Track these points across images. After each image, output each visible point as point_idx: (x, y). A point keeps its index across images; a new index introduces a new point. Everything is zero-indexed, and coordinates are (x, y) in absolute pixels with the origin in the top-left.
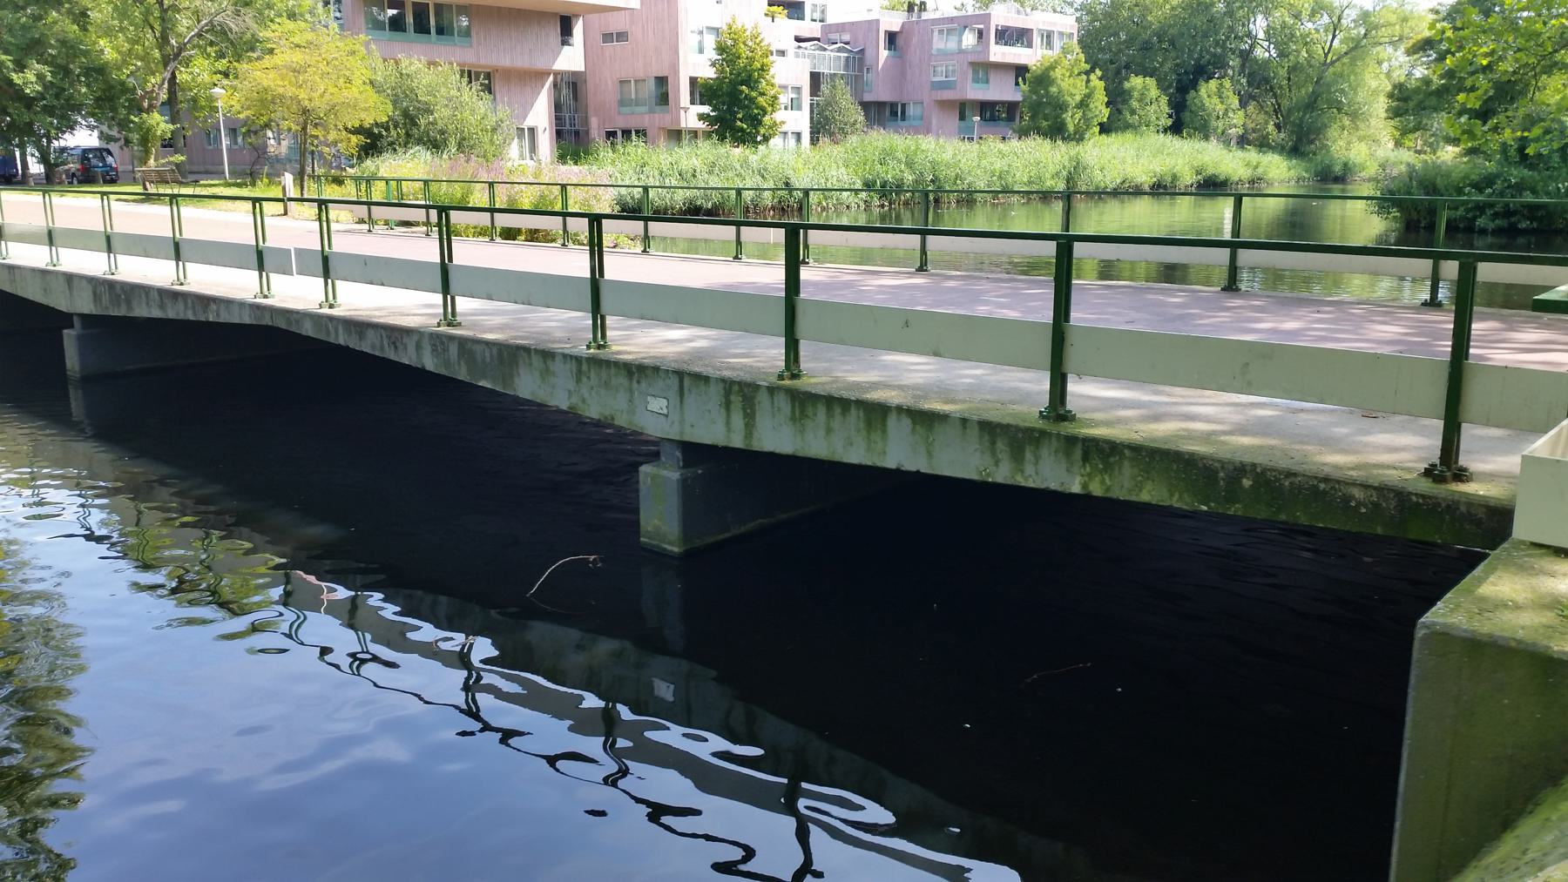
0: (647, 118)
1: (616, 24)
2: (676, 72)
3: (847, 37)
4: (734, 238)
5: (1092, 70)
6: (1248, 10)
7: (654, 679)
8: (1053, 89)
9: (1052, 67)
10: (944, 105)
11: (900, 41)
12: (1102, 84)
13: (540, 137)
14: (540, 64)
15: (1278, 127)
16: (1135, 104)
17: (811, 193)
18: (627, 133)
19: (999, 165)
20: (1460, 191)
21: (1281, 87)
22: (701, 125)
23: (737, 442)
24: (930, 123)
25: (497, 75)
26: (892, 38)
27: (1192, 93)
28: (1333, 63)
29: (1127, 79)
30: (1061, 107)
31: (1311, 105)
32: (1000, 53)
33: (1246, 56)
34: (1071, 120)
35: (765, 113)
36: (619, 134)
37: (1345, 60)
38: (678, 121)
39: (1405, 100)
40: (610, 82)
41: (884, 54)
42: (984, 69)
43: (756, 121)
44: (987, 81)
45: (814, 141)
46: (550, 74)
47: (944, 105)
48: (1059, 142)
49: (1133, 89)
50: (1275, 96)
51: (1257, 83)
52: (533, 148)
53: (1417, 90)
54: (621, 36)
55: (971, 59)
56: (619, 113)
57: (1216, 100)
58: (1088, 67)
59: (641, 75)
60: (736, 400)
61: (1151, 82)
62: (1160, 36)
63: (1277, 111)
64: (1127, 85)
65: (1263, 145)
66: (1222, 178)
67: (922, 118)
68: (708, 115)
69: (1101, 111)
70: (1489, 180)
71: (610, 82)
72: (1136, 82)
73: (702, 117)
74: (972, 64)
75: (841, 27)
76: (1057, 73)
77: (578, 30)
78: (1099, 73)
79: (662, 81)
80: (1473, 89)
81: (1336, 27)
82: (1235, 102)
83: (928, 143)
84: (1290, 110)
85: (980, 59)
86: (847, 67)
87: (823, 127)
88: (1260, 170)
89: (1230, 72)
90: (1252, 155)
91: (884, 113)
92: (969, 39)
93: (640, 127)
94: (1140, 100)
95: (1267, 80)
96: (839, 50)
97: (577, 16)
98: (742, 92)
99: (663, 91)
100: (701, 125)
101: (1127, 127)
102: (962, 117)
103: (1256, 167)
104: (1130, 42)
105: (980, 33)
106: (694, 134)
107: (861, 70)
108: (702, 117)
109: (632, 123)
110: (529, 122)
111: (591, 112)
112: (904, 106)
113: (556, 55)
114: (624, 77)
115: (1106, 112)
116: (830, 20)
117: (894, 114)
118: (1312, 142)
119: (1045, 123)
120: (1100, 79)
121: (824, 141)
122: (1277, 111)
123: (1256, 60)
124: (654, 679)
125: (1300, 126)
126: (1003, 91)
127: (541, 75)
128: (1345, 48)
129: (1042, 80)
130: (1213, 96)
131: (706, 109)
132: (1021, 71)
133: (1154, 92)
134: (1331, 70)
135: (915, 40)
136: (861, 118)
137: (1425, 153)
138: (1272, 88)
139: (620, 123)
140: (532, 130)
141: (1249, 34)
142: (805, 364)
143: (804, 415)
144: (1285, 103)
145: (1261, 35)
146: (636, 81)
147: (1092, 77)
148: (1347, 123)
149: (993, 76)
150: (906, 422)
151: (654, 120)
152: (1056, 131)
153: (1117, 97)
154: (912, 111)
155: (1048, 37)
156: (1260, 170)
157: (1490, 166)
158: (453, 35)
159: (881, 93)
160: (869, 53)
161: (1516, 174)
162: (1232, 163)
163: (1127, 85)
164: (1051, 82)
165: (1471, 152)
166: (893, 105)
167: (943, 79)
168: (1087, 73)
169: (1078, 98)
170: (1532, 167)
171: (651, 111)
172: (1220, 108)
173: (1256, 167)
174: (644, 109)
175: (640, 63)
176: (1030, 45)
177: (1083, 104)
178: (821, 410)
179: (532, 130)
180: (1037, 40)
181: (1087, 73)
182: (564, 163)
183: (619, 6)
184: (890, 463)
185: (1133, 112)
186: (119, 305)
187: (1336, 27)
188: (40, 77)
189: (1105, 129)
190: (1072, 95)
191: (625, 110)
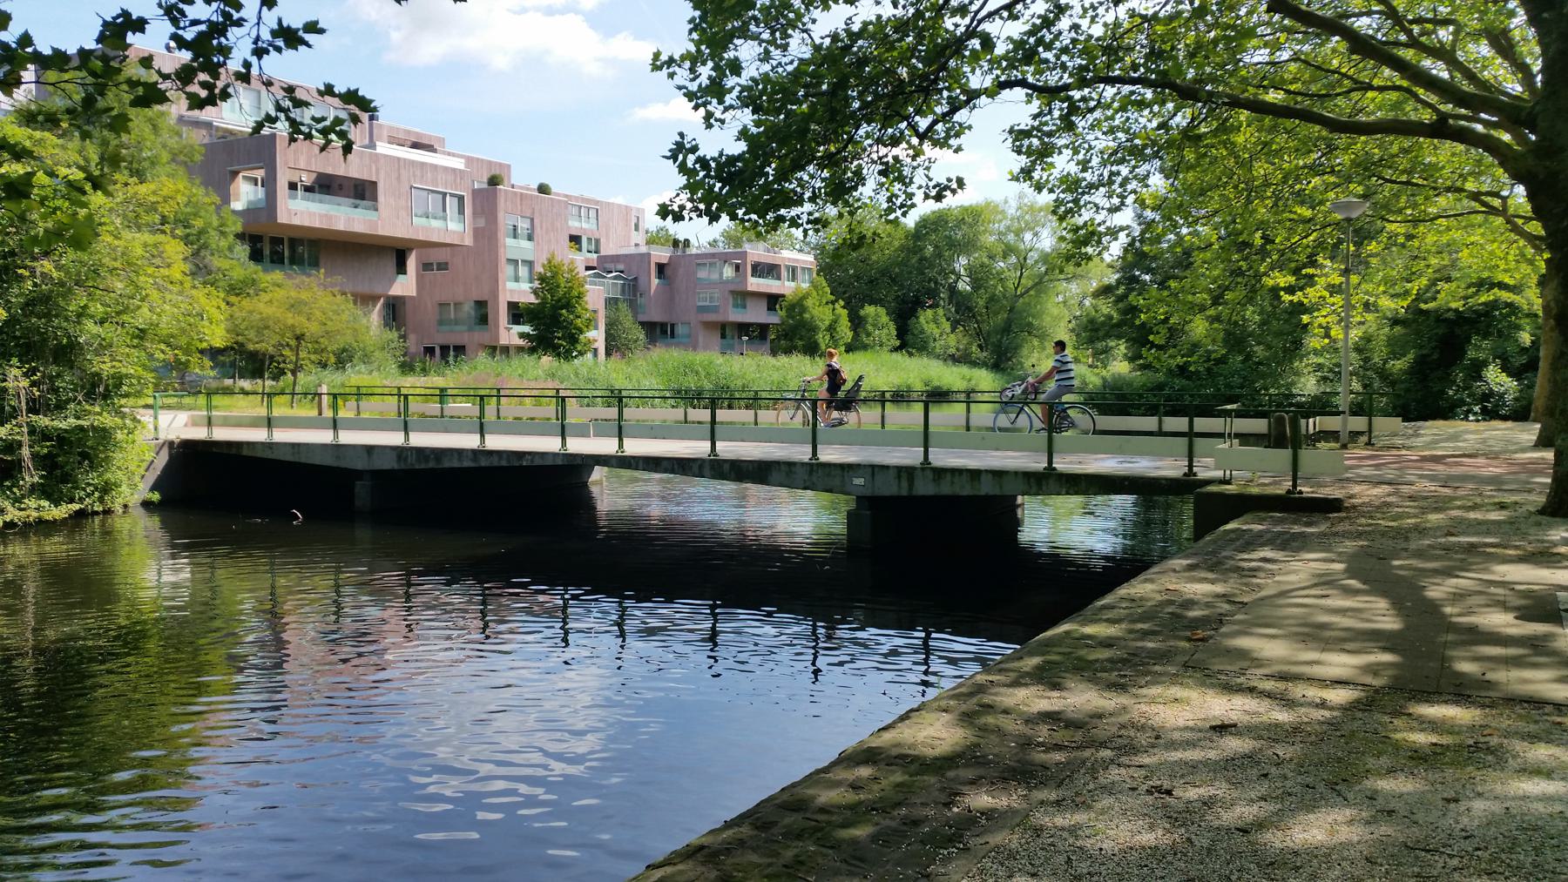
0: (466, 334)
1: (436, 256)
2: (496, 297)
3: (621, 267)
4: (708, 419)
5: (836, 301)
8: (807, 316)
9: (805, 297)
10: (709, 325)
11: (668, 272)
12: (846, 311)
14: (378, 290)
15: (980, 346)
16: (870, 328)
18: (445, 349)
19: (776, 376)
20: (1141, 396)
21: (981, 315)
22: (521, 342)
23: (904, 492)
24: (697, 341)
26: (661, 268)
27: (913, 320)
28: (1022, 295)
29: (862, 307)
30: (813, 329)
31: (1007, 329)
32: (755, 284)
33: (952, 290)
34: (822, 339)
35: (581, 332)
36: (438, 351)
37: (1032, 293)
38: (497, 338)
39: (1097, 330)
40: (429, 305)
41: (655, 281)
42: (743, 297)
43: (573, 340)
44: (745, 307)
45: (608, 354)
46: (379, 298)
47: (709, 325)
48: (817, 359)
49: (867, 316)
50: (977, 322)
51: (963, 310)
53: (1103, 323)
55: (732, 288)
57: (932, 325)
58: (833, 298)
59: (460, 299)
60: (904, 475)
61: (882, 311)
62: (884, 272)
63: (979, 333)
64: (862, 313)
65: (974, 364)
66: (945, 388)
67: (689, 336)
68: (528, 334)
69: (845, 332)
70: (1160, 387)
71: (429, 305)
72: (869, 310)
73: (522, 336)
74: (732, 292)
75: (616, 259)
76: (809, 303)
77: (412, 263)
78: (842, 303)
79: (481, 305)
80: (1158, 333)
81: (1022, 266)
82: (947, 326)
83: (700, 357)
84: (989, 333)
85: (739, 288)
86: (623, 292)
87: (614, 345)
88: (973, 382)
89: (942, 303)
90: (964, 370)
91: (659, 332)
92: (728, 272)
93: (459, 342)
94: (873, 325)
95: (970, 309)
96: (615, 278)
98: (561, 315)
99: (483, 314)
100: (521, 342)
101: (865, 347)
102: (723, 336)
103: (970, 380)
104: (858, 277)
105: (737, 267)
106: (520, 349)
107: (635, 295)
108: (522, 336)
109: (452, 340)
112: (673, 326)
113: (392, 282)
115: (850, 334)
116: (603, 253)
117: (664, 332)
118: (1010, 359)
119: (800, 343)
120: (844, 307)
121: (615, 357)
122: (979, 333)
123: (960, 293)
125: (1000, 347)
126: (756, 314)
127: (375, 299)
128: (1030, 283)
129: (797, 306)
130: (932, 322)
131: (527, 329)
132: (773, 300)
133: (885, 319)
134: (1021, 300)
135: (681, 271)
136: (642, 336)
137: (1097, 367)
138: (974, 316)
139: (439, 339)
141: (953, 272)
142: (931, 457)
143: (939, 478)
144: (985, 327)
145: (963, 272)
147: (837, 306)
148: (1036, 343)
149: (749, 303)
150: (990, 476)
151: (480, 336)
152: (812, 350)
153: (857, 322)
154: (680, 330)
155: (793, 272)
156: (973, 382)
157: (1161, 377)
159: (655, 316)
160: (642, 281)
161: (1178, 383)
162: (952, 377)
163: (862, 313)
164: (804, 309)
165: (1143, 367)
166: (663, 326)
167: (707, 304)
168: (833, 303)
169: (827, 323)
170: (1189, 378)
171: (470, 330)
172: (936, 332)
173: (970, 380)
174: (465, 328)
175: (464, 292)
176: (779, 278)
177: (831, 329)
178: (949, 476)
179: (596, 350)
180: (784, 273)
181: (833, 303)
183: (442, 241)
184: (983, 493)
185: (868, 335)
187: (1022, 266)
189: (849, 349)
190: (822, 320)
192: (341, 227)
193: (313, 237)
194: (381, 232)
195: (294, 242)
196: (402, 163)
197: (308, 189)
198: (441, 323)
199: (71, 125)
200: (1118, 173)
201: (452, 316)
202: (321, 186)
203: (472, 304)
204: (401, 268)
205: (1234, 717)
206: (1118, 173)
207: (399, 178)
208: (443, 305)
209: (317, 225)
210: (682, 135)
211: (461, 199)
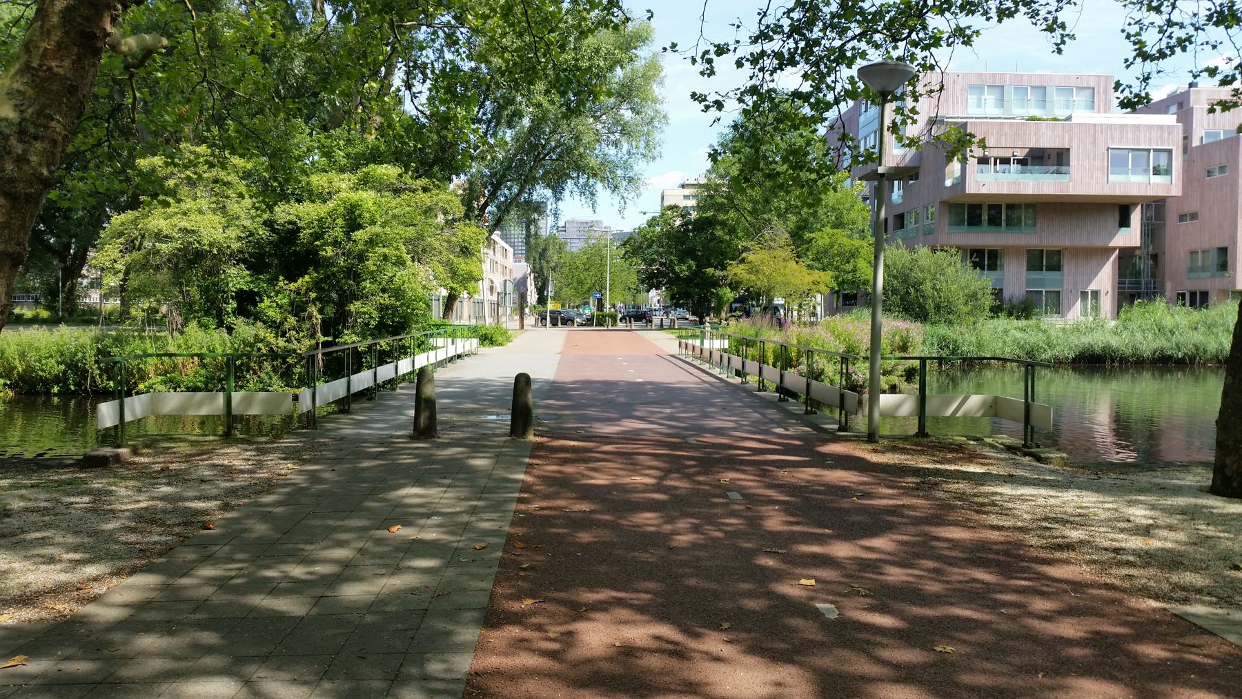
6: (110, 320)
7: (223, 642)
13: (1102, 298)
14: (1098, 242)
17: (928, 362)
25: (1066, 253)
38: (1234, 284)
52: (1096, 309)
54: (1194, 216)
56: (1188, 278)
59: (1206, 246)
77: (1136, 217)
97: (1136, 205)
110: (1093, 286)
111: (1167, 278)
113: (1112, 235)
114: (1193, 248)
124: (223, 642)
140: (1095, 294)
146: (1203, 252)
158: (1000, 225)
171: (1213, 276)
179: (1095, 294)
182: (484, 345)
186: (1122, 427)
188: (689, 268)
191: (1193, 275)
192: (1030, 191)
193: (1028, 201)
194: (1071, 192)
195: (1011, 207)
196: (1099, 129)
197: (1023, 162)
198: (1192, 269)
199: (510, 126)
200: (863, 55)
201: (1200, 264)
202: (1033, 158)
203: (1215, 252)
204: (1124, 222)
205: (990, 532)
206: (863, 55)
207: (1094, 143)
208: (1193, 253)
209: (1005, 191)
210: (1191, 72)
211: (1170, 151)
